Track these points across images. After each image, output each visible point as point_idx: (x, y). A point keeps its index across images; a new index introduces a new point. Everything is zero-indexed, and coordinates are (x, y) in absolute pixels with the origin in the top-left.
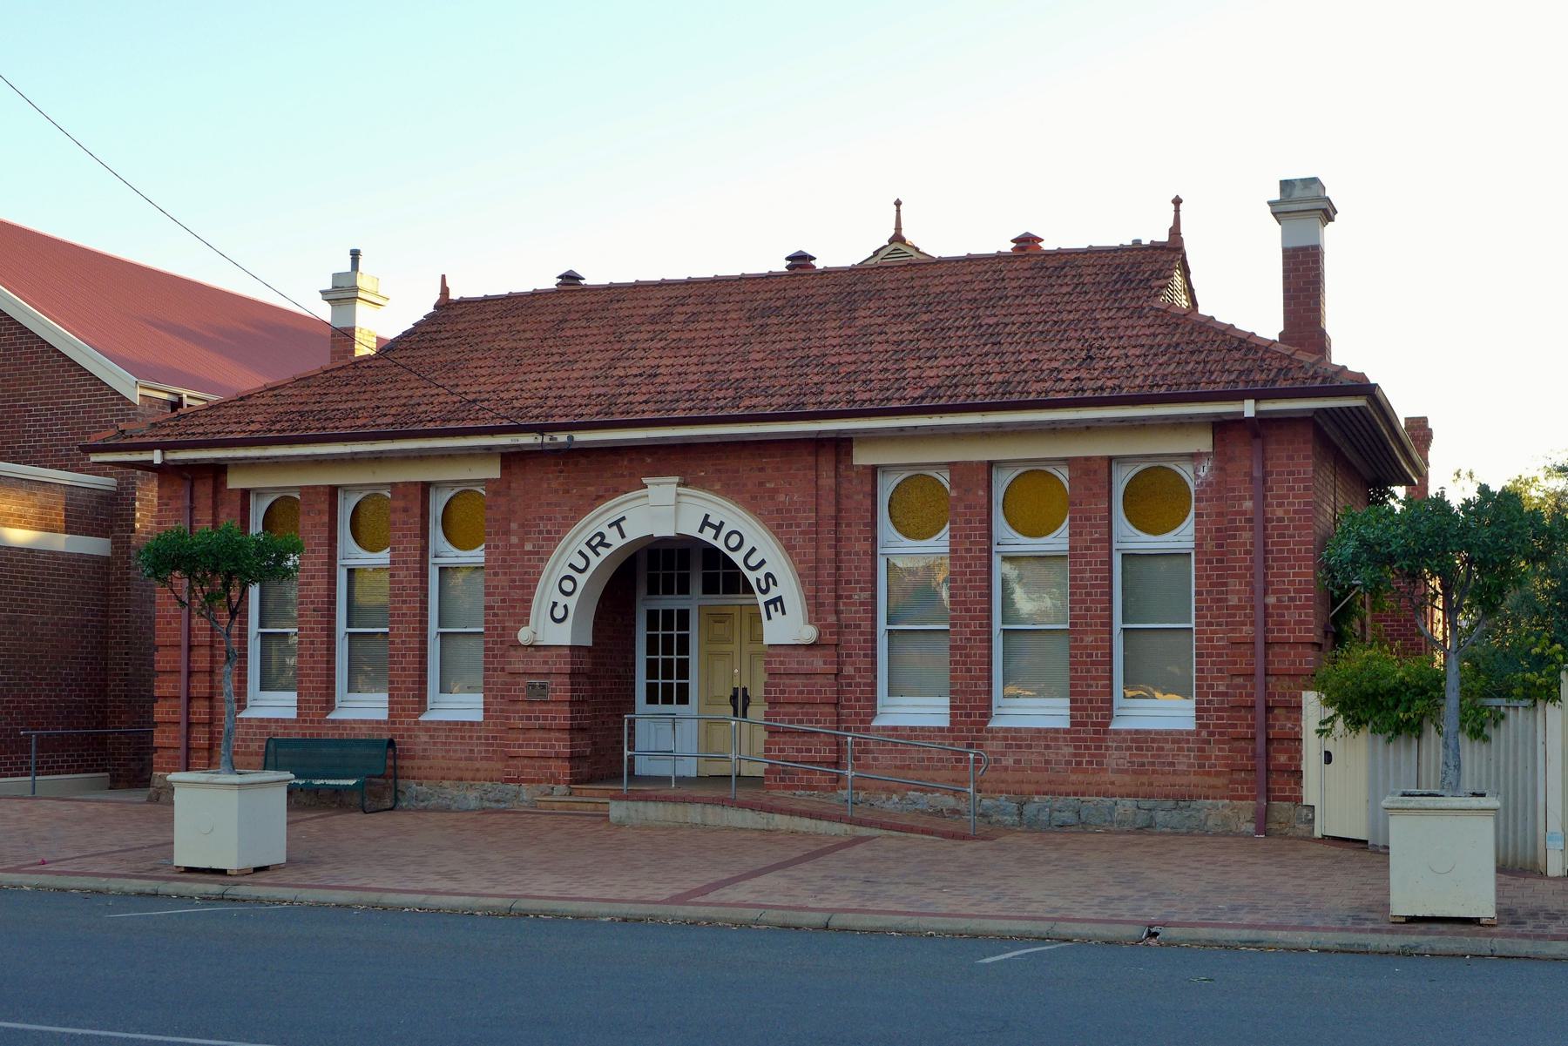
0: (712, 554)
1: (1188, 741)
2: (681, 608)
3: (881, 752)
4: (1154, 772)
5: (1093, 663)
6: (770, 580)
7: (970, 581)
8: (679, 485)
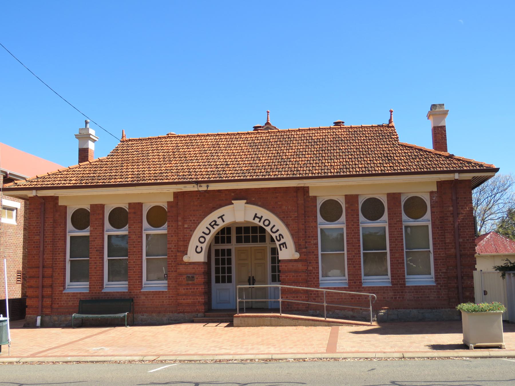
1: (433, 289)
6: (281, 236)
7: (354, 236)
8: (246, 203)
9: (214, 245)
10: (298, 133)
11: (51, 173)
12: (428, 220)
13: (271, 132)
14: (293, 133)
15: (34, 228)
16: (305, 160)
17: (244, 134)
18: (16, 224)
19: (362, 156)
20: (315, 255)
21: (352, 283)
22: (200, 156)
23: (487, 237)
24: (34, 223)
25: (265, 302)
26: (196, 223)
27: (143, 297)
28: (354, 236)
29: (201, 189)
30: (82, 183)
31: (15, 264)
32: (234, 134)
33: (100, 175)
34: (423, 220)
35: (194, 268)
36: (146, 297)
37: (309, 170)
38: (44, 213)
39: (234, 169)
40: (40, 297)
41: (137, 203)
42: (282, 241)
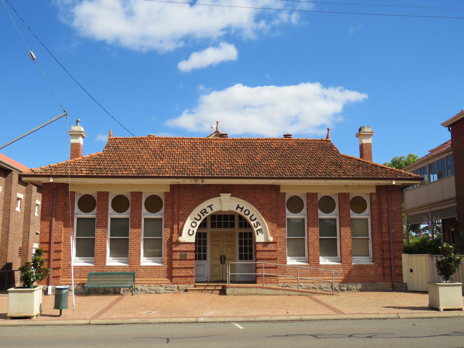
0: (241, 217)
1: (373, 267)
2: (245, 232)
3: (290, 272)
4: (364, 275)
5: (347, 247)
6: (258, 224)
7: (314, 225)
8: (231, 196)
11: (61, 164)
12: (304, 215)
15: (47, 210)
21: (312, 262)
24: (46, 205)
26: (189, 210)
27: (142, 271)
29: (197, 183)
34: (364, 215)
36: (145, 271)
41: (138, 192)
42: (259, 227)
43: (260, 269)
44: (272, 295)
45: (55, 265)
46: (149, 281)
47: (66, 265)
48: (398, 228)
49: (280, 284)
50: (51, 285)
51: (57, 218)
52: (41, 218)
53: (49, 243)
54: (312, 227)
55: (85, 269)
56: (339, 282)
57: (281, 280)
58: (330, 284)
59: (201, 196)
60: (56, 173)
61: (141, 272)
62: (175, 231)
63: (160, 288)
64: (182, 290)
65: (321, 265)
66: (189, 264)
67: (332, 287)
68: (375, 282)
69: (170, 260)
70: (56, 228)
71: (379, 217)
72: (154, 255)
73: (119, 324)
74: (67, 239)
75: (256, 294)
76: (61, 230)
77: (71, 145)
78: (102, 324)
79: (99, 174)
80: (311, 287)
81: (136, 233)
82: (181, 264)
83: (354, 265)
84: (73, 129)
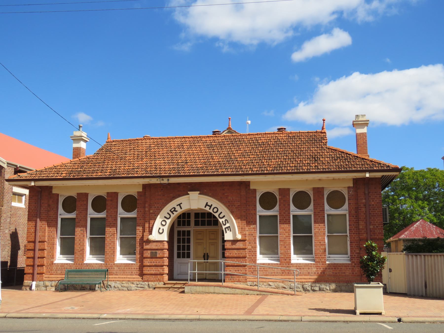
1: (349, 266)
6: (226, 221)
7: (285, 222)
8: (199, 194)
9: (177, 227)
10: (248, 137)
12: (346, 210)
13: (219, 136)
14: (244, 137)
15: (33, 211)
16: (249, 160)
17: (204, 137)
18: (25, 207)
19: (295, 157)
20: (253, 237)
22: (166, 155)
23: (417, 224)
24: (33, 207)
25: (216, 274)
26: (159, 209)
27: (116, 268)
28: (285, 222)
29: (162, 182)
30: (70, 176)
31: (22, 239)
32: (196, 137)
33: (86, 170)
35: (157, 246)
36: (119, 268)
37: (250, 168)
38: (41, 200)
39: (191, 167)
40: (36, 267)
42: (228, 225)
43: (229, 267)
44: (230, 294)
45: (39, 262)
46: (122, 278)
47: (49, 262)
48: (377, 224)
49: (248, 282)
50: (35, 281)
51: (42, 219)
52: (28, 219)
53: (34, 242)
54: (284, 224)
55: (66, 266)
56: (311, 282)
57: (250, 278)
58: (301, 283)
59: (171, 195)
60: (193, 173)
61: (116, 269)
62: (147, 229)
63: (132, 285)
64: (152, 287)
65: (292, 264)
66: (159, 262)
67: (303, 287)
68: (351, 282)
69: (142, 258)
70: (40, 228)
71: (356, 212)
72: (129, 253)
73: (30, 318)
74: (50, 238)
75: (214, 293)
76: (45, 230)
77: (74, 149)
78: (16, 318)
79: (75, 176)
80: (280, 286)
81: (111, 232)
82: (151, 262)
83: (329, 264)
84: (74, 134)
